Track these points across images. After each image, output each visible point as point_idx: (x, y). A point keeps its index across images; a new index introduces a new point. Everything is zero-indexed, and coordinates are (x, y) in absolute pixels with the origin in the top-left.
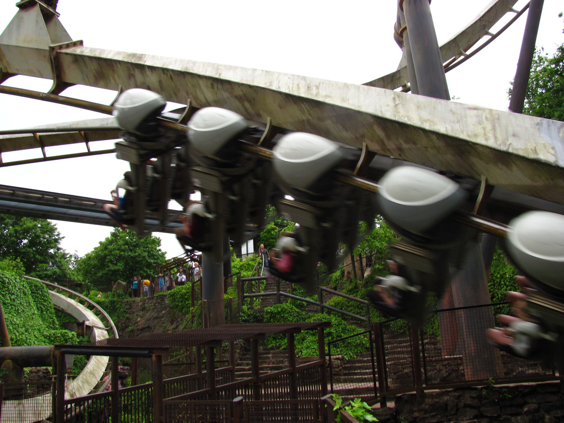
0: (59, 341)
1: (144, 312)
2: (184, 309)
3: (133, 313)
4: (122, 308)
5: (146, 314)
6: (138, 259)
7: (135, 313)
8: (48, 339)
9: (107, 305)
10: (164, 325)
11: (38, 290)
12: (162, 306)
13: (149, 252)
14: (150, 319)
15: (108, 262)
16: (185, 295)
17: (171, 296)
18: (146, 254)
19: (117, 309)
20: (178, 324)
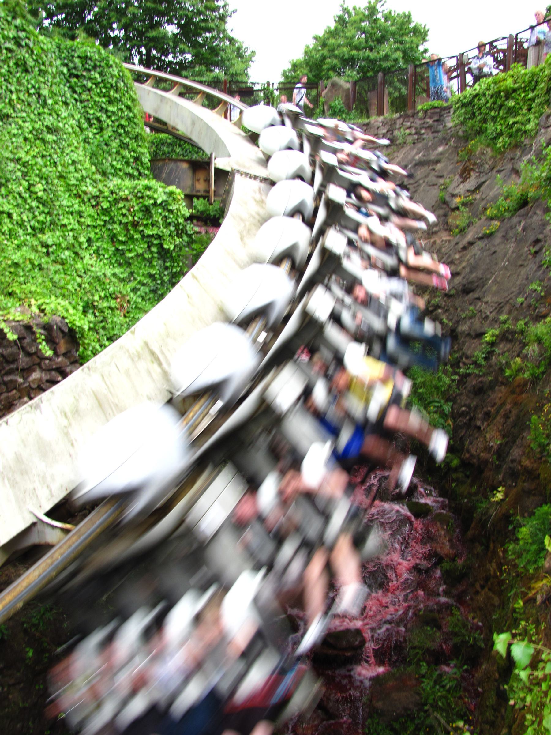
0: (124, 211)
2: (501, 140)
5: (396, 155)
6: (385, 65)
8: (93, 206)
10: (441, 181)
11: (89, 70)
12: (436, 135)
13: (405, 52)
15: (328, 70)
17: (464, 105)
18: (399, 54)
20: (483, 180)
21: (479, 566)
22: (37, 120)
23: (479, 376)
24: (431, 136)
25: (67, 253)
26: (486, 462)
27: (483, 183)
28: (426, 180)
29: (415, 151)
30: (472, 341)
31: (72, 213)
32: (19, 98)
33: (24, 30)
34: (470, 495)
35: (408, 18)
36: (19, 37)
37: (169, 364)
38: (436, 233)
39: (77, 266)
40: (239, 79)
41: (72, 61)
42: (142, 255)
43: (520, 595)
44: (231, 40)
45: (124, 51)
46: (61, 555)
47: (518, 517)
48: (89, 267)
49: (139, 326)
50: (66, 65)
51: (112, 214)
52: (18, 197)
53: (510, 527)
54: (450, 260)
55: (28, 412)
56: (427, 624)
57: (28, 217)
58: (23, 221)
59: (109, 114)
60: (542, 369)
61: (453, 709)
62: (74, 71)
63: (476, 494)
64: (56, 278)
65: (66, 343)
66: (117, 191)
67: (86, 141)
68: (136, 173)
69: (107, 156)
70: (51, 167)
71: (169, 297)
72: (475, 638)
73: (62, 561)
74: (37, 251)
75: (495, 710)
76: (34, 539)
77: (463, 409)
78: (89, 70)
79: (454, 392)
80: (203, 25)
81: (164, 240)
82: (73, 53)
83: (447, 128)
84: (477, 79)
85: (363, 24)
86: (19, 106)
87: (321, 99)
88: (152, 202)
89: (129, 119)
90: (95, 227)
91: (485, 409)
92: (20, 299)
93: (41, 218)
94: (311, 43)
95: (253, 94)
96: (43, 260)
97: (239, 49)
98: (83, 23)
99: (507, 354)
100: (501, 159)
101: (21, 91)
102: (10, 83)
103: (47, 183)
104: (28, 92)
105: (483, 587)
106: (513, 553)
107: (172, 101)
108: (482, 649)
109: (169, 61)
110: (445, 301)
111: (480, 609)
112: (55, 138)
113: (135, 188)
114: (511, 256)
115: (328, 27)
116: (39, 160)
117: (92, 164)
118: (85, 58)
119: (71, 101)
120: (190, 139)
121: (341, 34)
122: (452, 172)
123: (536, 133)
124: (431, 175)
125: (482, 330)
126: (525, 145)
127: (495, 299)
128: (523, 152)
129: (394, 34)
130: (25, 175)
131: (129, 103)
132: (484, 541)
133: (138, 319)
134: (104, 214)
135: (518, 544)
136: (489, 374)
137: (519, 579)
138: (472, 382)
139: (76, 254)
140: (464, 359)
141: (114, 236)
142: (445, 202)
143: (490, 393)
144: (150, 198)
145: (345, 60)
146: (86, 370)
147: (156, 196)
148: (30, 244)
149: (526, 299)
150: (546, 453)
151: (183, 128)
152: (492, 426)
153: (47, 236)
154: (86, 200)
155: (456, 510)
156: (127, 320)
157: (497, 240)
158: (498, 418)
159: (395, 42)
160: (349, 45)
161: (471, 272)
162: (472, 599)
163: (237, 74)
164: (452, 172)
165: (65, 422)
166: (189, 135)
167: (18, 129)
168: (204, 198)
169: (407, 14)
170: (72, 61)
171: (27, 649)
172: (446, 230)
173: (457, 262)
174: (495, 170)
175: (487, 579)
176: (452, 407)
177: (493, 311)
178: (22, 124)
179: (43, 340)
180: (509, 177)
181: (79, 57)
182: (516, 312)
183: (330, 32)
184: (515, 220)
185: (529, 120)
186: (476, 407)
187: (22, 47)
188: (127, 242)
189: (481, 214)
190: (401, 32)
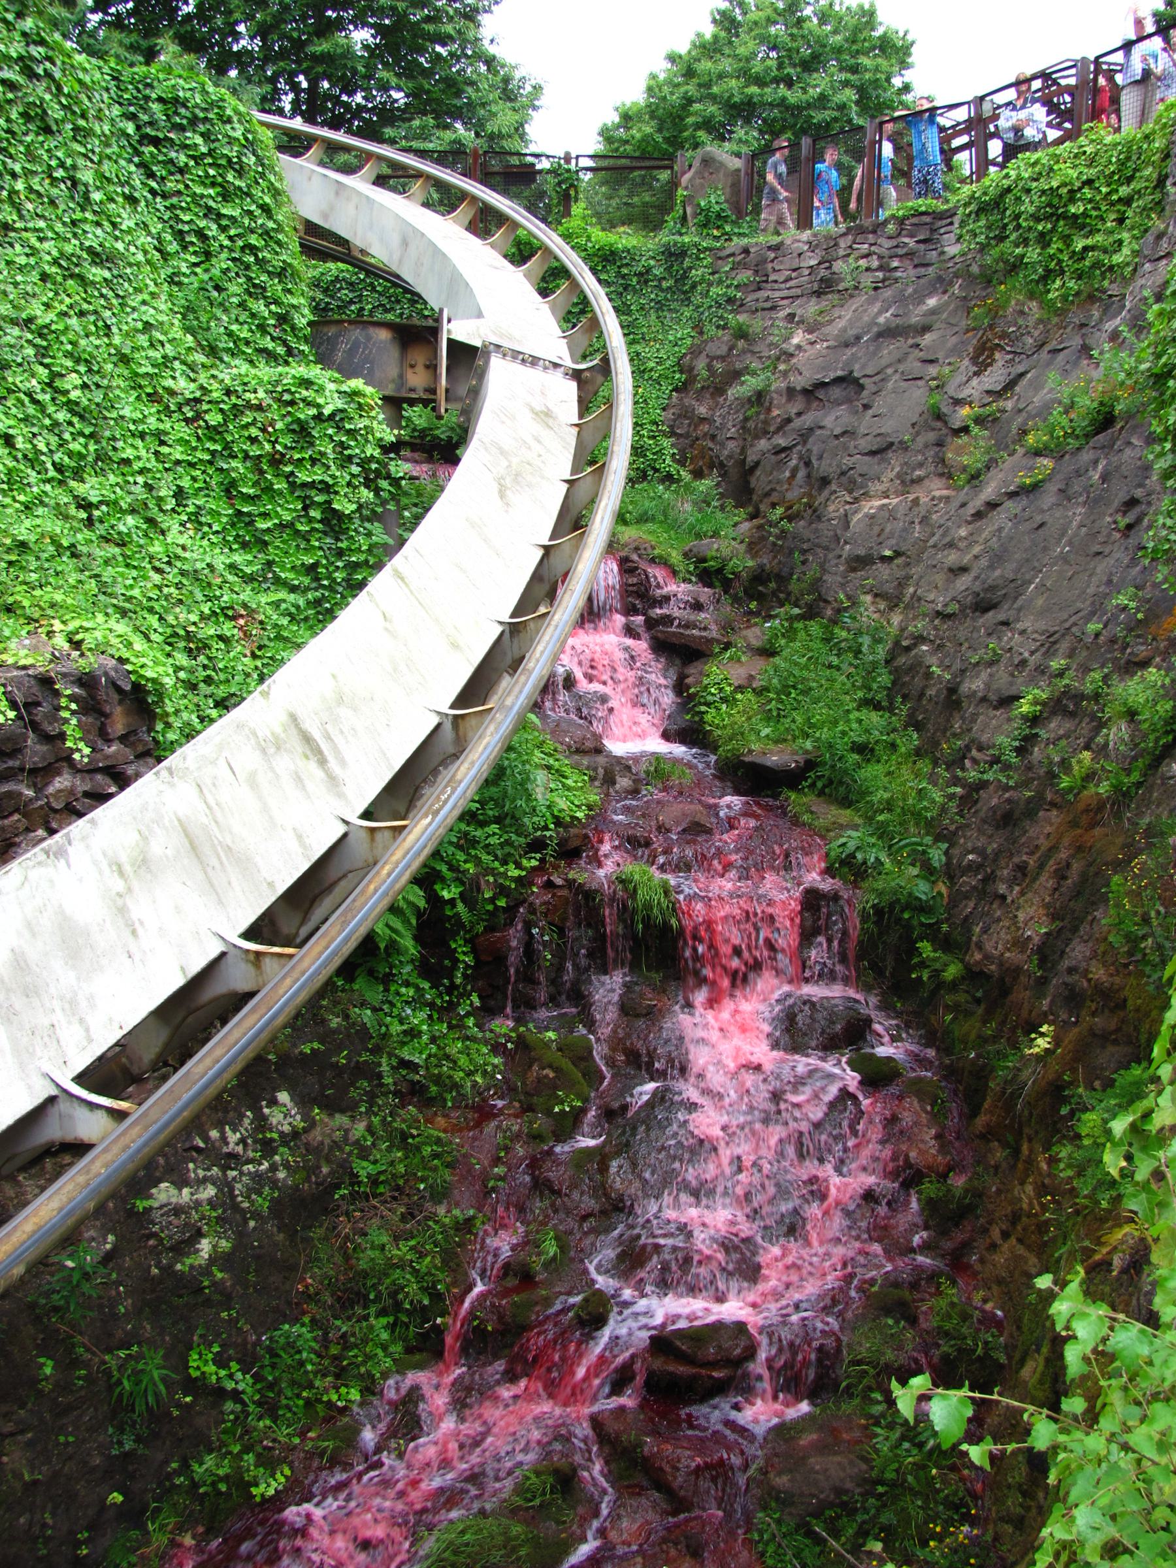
0: (254, 432)
1: (824, 303)
2: (1058, 283)
3: (773, 308)
4: (720, 282)
6: (818, 116)
7: (783, 307)
8: (187, 421)
9: (648, 270)
10: (933, 370)
12: (922, 271)
13: (861, 90)
14: (858, 338)
15: (698, 126)
16: (1072, 197)
18: (850, 95)
19: (694, 286)
20: (1020, 369)
21: (999, 1191)
22: (69, 236)
23: (1007, 788)
24: (912, 272)
25: (130, 520)
26: (1017, 971)
27: (1022, 375)
28: (901, 368)
29: (878, 305)
30: (992, 713)
31: (142, 436)
32: (30, 189)
33: (42, 42)
34: (983, 1040)
35: (868, 17)
36: (32, 58)
37: (343, 763)
38: (920, 480)
39: (151, 549)
40: (507, 144)
41: (145, 110)
42: (291, 525)
43: (1079, 1256)
44: (490, 61)
45: (260, 84)
46: (107, 1165)
47: (1080, 1090)
48: (179, 551)
49: (281, 679)
50: (132, 117)
51: (229, 438)
52: (26, 400)
53: (1064, 1111)
54: (948, 539)
55: (39, 863)
56: (888, 1312)
57: (48, 444)
58: (38, 452)
59: (224, 222)
60: (1135, 776)
61: (938, 1491)
62: (149, 130)
63: (995, 1039)
64: (108, 574)
65: (128, 713)
66: (240, 389)
67: (172, 280)
68: (281, 350)
69: (219, 313)
70: (98, 337)
71: (346, 617)
72: (986, 1343)
73: (109, 1177)
74: (66, 517)
75: (1025, 1494)
76: (51, 1131)
77: (970, 857)
78: (181, 128)
79: (952, 821)
80: (430, 28)
81: (336, 493)
82: (148, 92)
83: (946, 257)
84: (1010, 152)
85: (773, 30)
86: (30, 206)
87: (680, 192)
88: (313, 412)
89: (266, 234)
90: (192, 465)
91: (1016, 860)
92: (30, 620)
93: (75, 446)
94: (662, 68)
95: (534, 180)
96: (79, 536)
97: (507, 80)
98: (172, 20)
99: (1063, 742)
100: (1060, 327)
101: (35, 173)
102: (11, 157)
103: (90, 371)
104: (50, 176)
105: (1005, 1235)
106: (1069, 1166)
107: (359, 193)
108: (1002, 1366)
109: (358, 105)
110: (936, 628)
111: (1000, 1281)
112: (107, 275)
113: (278, 382)
114: (1076, 535)
115: (698, 35)
116: (74, 322)
117: (188, 330)
118: (173, 103)
119: (141, 193)
120: (398, 277)
121: (727, 51)
122: (955, 351)
123: (1135, 270)
124: (911, 357)
125: (1013, 691)
126: (1110, 296)
127: (1042, 625)
128: (1105, 312)
129: (839, 50)
130: (42, 353)
131: (267, 199)
132: (1010, 1138)
133: (282, 662)
134: (211, 439)
135: (1079, 1147)
136: (1025, 784)
137: (1079, 1219)
138: (991, 800)
139: (151, 521)
140: (974, 753)
141: (233, 484)
142: (939, 416)
143: (1027, 823)
144: (309, 404)
145: (734, 106)
146: (164, 773)
147: (321, 401)
148: (52, 502)
149: (1105, 626)
150: (1139, 956)
151: (381, 252)
152: (1029, 895)
153: (87, 486)
154: (173, 408)
155: (950, 1073)
156: (259, 663)
157: (1048, 498)
158: (1042, 879)
159: (841, 70)
160: (744, 73)
161: (991, 567)
162: (982, 1261)
163: (501, 136)
164: (955, 351)
165: (119, 885)
166: (394, 268)
167: (27, 255)
168: (426, 403)
169: (867, 7)
170: (145, 110)
171: (42, 1360)
172: (941, 475)
173: (962, 545)
174: (1047, 348)
175: (1015, 1218)
176: (946, 853)
177: (1036, 650)
178: (37, 245)
179: (73, 713)
180: (1076, 364)
181: (160, 100)
182: (1084, 653)
183: (703, 46)
184: (1086, 456)
185: (1120, 242)
186: (997, 854)
187: (37, 77)
188: (258, 497)
189: (1014, 442)
190: (854, 47)
